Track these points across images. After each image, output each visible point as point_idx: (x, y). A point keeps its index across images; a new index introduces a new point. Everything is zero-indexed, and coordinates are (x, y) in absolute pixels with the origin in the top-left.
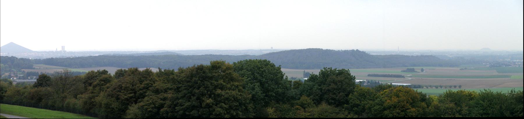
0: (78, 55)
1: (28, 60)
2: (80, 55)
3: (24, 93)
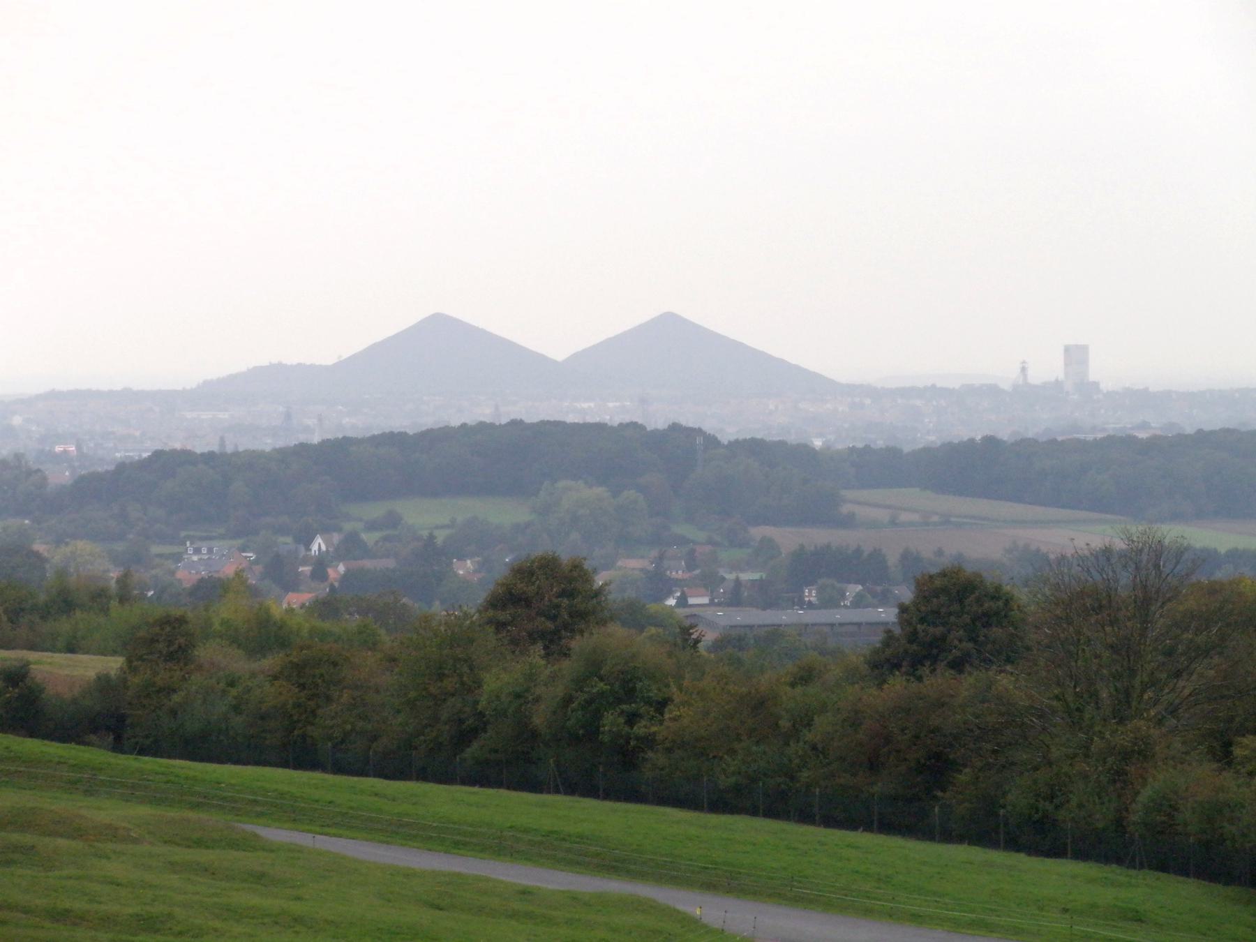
0: (1190, 421)
1: (801, 455)
2: (1214, 420)
3: (804, 720)
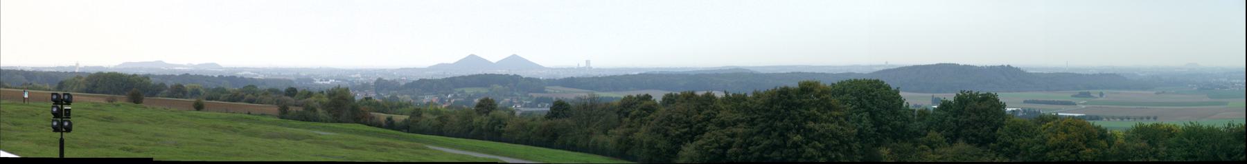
1: (538, 80)
